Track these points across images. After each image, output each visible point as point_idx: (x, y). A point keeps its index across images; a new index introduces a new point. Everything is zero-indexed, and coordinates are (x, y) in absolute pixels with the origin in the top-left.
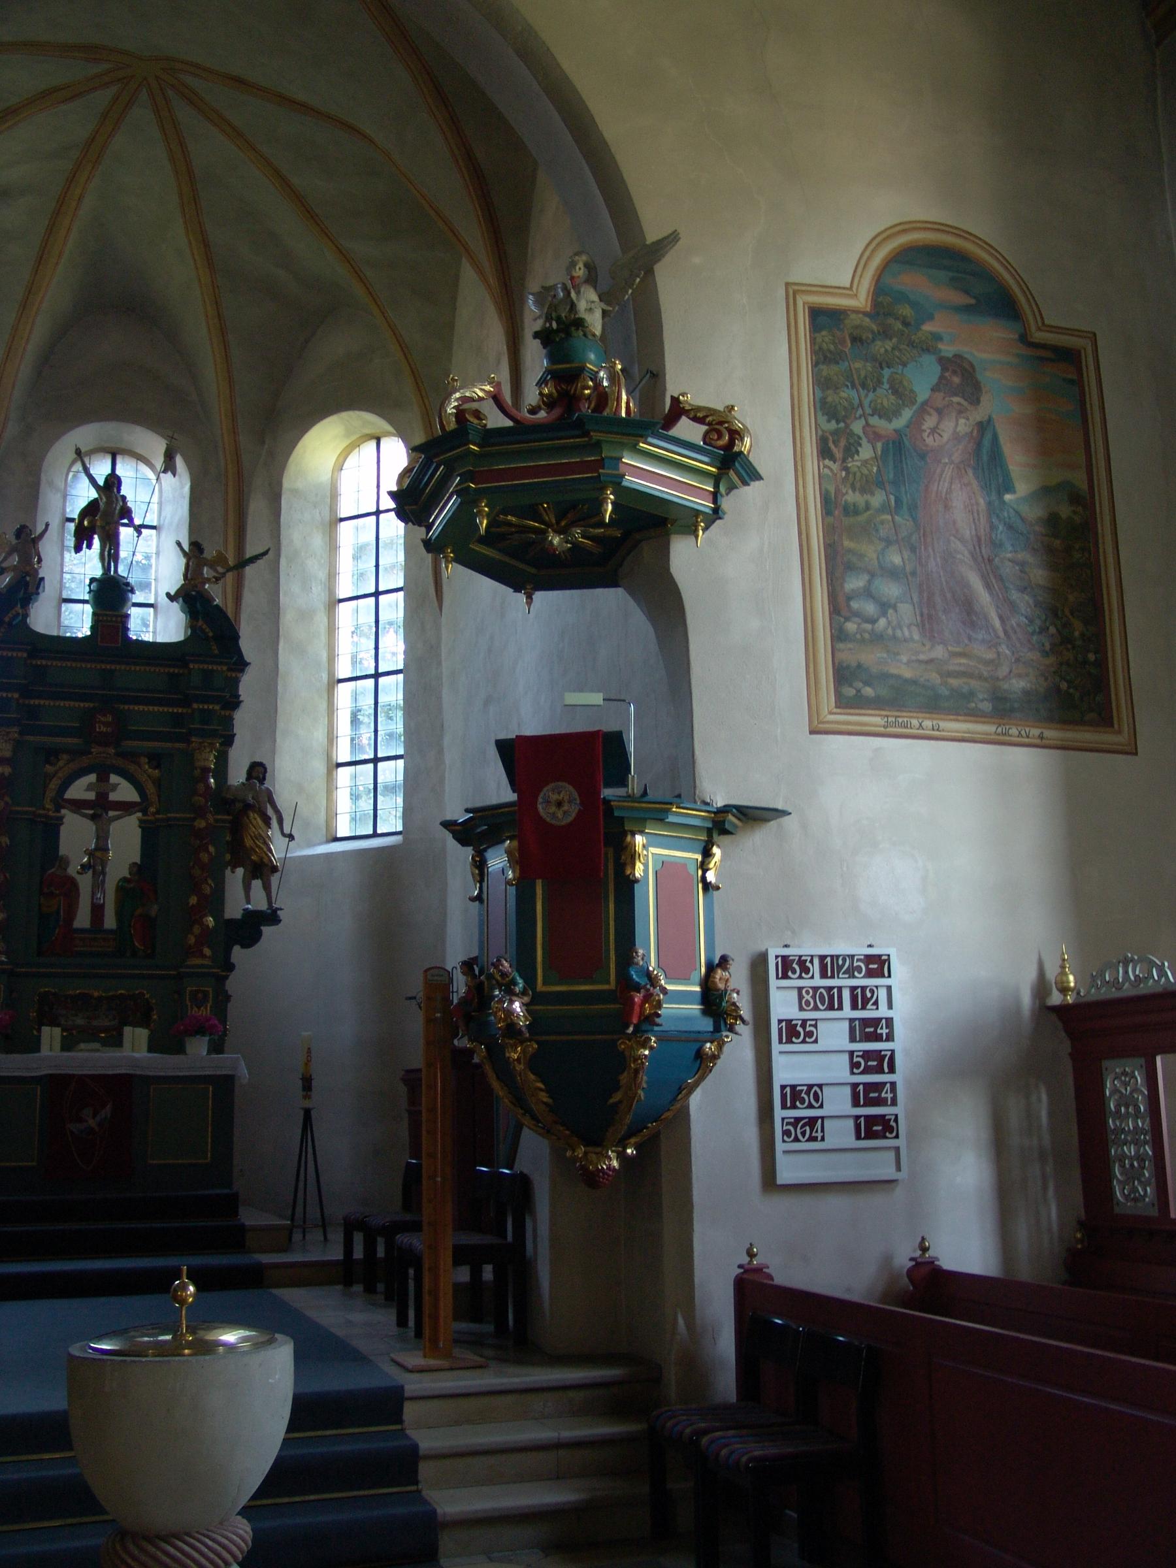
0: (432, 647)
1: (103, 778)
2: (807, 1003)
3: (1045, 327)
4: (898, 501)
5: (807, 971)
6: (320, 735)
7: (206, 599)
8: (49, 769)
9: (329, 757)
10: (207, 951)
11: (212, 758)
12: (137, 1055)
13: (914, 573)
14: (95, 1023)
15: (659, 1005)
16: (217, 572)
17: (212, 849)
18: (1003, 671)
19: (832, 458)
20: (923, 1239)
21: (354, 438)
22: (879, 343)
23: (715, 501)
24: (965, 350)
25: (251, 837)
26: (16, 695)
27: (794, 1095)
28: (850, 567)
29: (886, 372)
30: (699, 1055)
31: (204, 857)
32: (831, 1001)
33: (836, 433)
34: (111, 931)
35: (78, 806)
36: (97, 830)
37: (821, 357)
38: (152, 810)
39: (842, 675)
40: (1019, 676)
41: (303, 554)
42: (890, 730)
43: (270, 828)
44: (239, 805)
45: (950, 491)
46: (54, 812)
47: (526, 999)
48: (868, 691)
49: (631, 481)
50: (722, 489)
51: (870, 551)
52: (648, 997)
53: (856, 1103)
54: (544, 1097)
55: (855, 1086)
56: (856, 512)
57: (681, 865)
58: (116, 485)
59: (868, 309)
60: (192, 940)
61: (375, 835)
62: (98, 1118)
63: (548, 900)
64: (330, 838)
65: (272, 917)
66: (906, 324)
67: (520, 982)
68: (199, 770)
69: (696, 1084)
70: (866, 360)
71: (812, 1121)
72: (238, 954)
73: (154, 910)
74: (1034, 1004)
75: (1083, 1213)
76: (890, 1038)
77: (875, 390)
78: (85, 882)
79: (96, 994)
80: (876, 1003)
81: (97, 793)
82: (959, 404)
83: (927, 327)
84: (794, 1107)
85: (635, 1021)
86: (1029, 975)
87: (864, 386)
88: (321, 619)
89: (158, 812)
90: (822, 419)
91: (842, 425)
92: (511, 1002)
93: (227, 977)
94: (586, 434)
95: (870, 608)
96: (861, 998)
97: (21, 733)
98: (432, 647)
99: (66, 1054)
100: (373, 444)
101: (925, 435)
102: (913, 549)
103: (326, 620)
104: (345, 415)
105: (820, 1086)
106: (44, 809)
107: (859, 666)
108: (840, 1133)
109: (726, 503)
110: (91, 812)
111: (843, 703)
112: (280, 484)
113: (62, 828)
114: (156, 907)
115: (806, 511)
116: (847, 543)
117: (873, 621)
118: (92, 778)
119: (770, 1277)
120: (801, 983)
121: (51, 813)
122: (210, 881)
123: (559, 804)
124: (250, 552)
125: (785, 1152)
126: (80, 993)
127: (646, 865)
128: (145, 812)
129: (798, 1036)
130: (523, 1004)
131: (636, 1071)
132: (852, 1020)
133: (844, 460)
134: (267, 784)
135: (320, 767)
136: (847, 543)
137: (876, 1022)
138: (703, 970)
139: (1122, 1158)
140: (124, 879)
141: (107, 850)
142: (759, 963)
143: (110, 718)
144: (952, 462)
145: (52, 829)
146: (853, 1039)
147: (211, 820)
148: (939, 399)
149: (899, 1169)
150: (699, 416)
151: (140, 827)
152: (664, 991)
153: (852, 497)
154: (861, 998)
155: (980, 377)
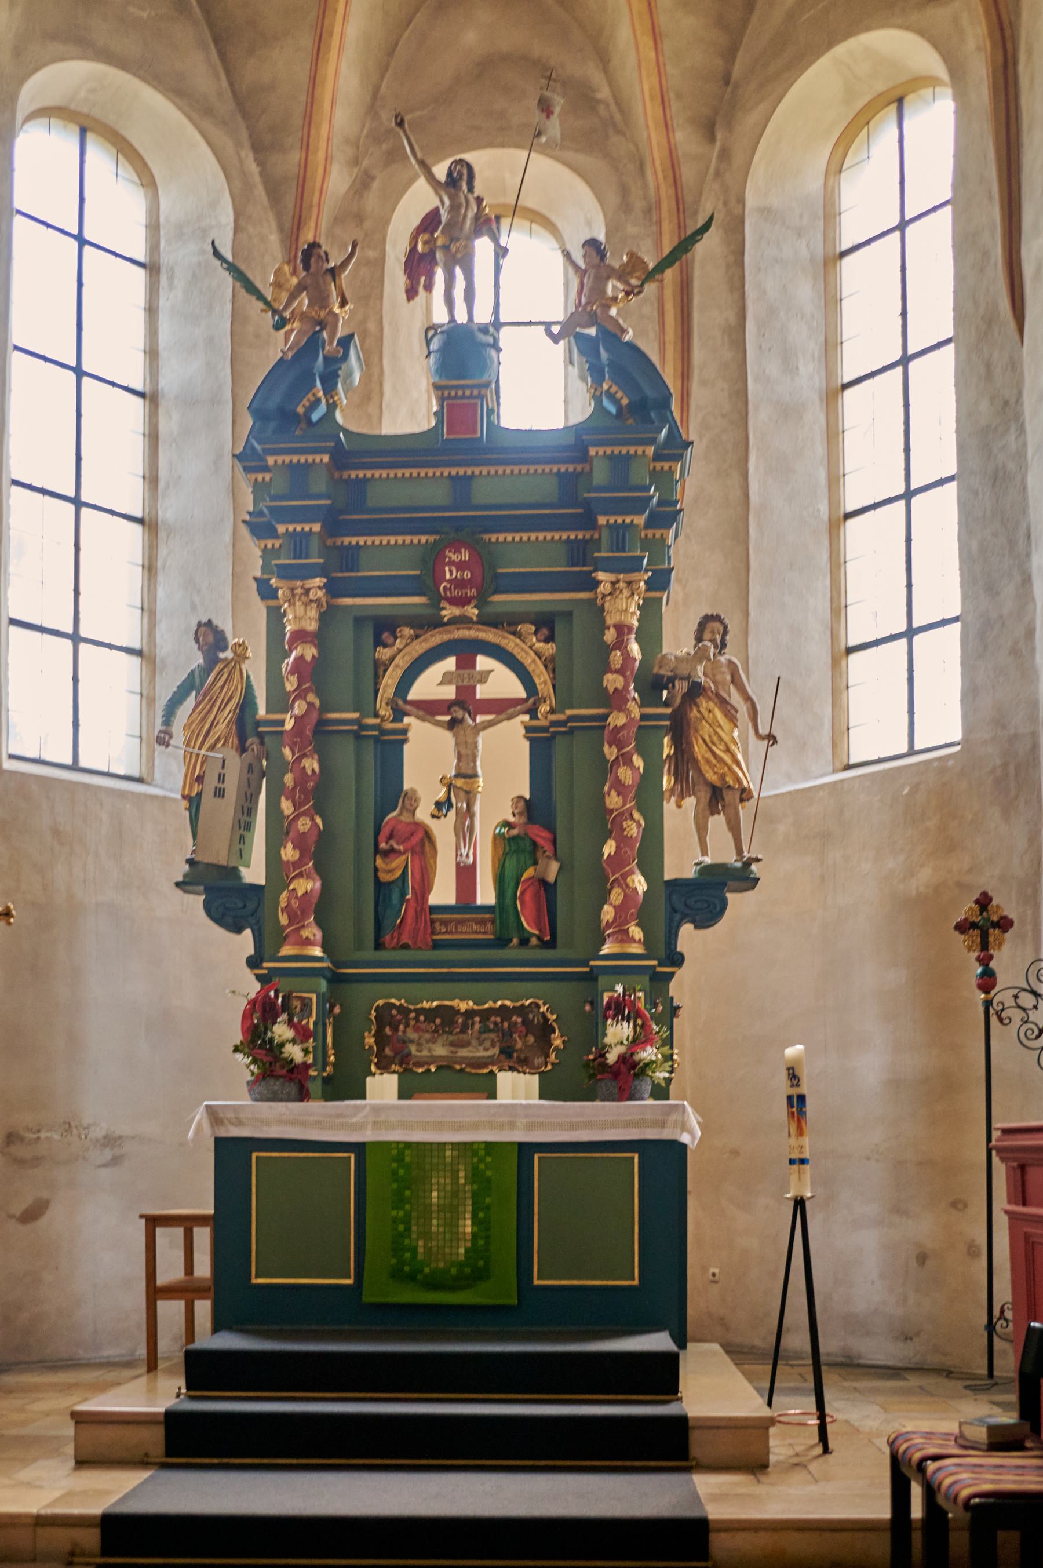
0: (1006, 403)
1: (466, 663)
7: (611, 335)
8: (383, 653)
11: (633, 608)
14: (463, 1053)
16: (627, 283)
25: (705, 742)
26: (317, 527)
31: (625, 774)
38: (544, 708)
41: (782, 314)
43: (736, 726)
44: (681, 687)
46: (393, 721)
58: (465, 177)
61: (912, 752)
64: (838, 765)
68: (612, 630)
72: (688, 936)
73: (552, 870)
78: (443, 830)
79: (463, 1006)
81: (458, 688)
88: (815, 415)
89: (552, 711)
93: (671, 975)
97: (333, 589)
98: (1006, 403)
103: (822, 418)
106: (376, 715)
110: (447, 718)
113: (406, 747)
114: (554, 866)
118: (450, 663)
122: (637, 815)
126: (437, 1007)
128: (533, 712)
135: (819, 652)
141: (475, 776)
143: (465, 556)
151: (527, 738)
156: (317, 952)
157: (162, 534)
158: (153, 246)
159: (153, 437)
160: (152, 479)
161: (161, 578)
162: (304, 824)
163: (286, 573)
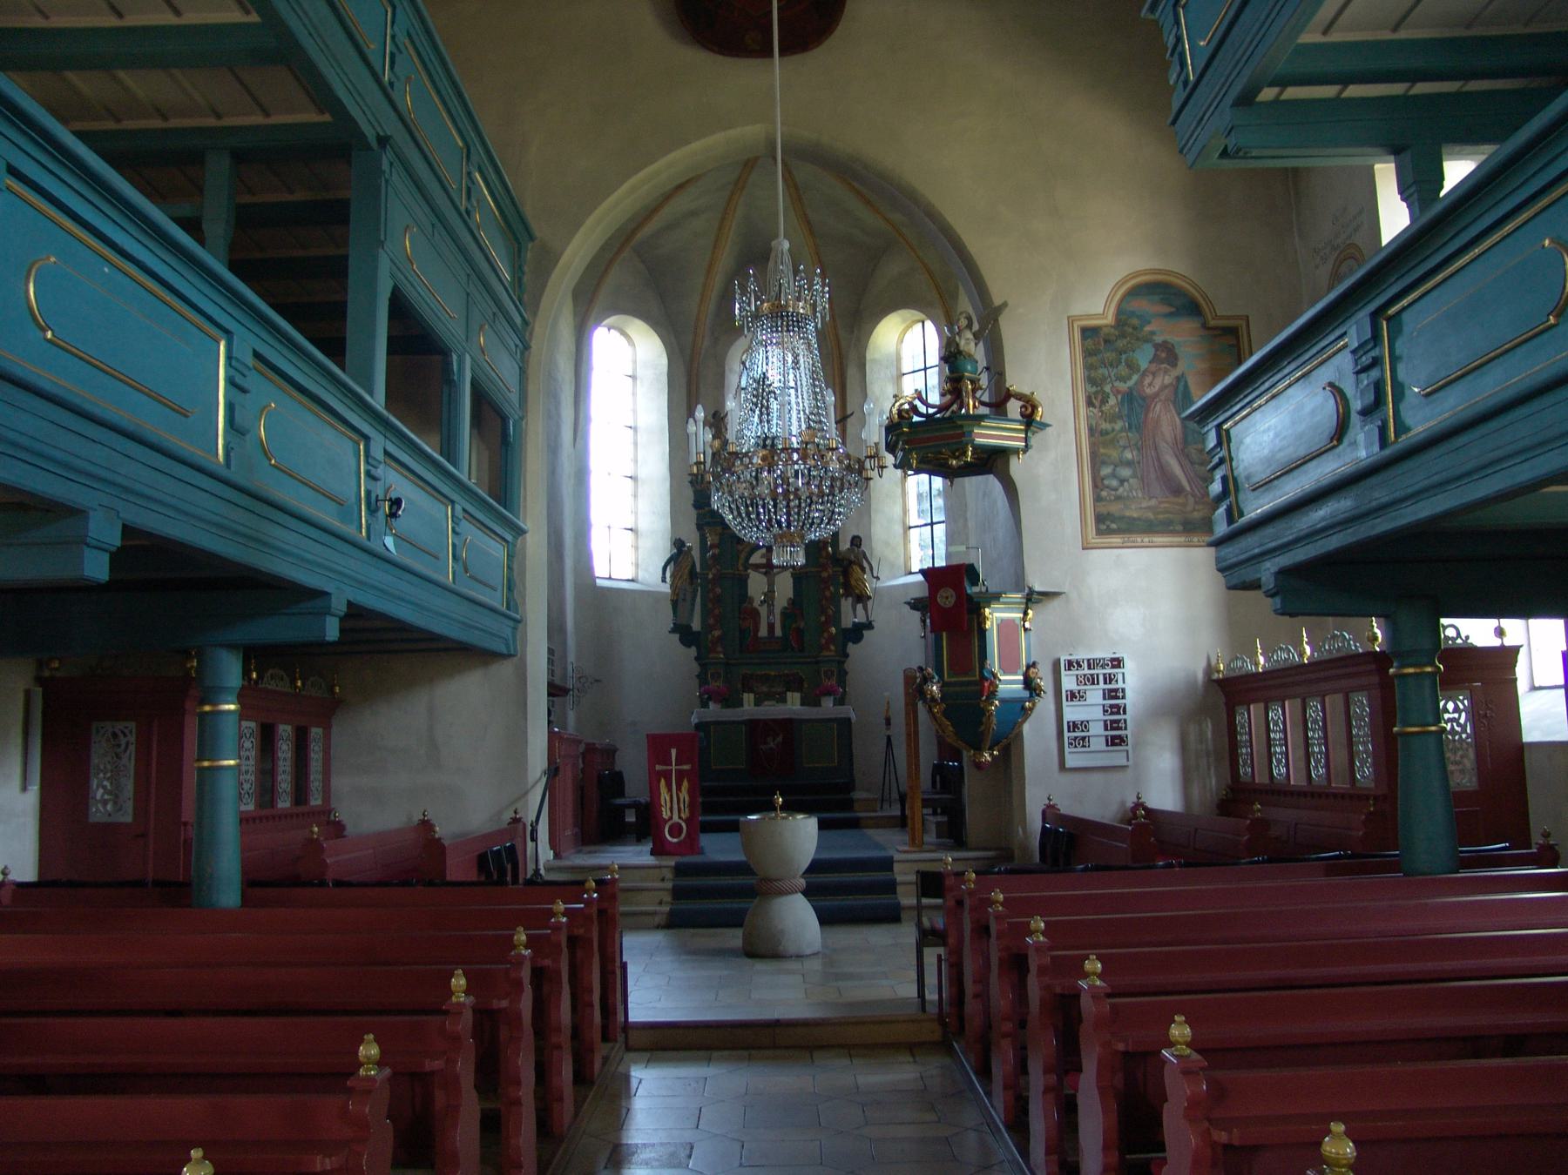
2: (1081, 682)
3: (1216, 317)
4: (1130, 427)
5: (1081, 667)
6: (898, 510)
9: (904, 523)
10: (833, 648)
12: (794, 708)
13: (1139, 463)
14: (773, 690)
15: (997, 686)
17: (832, 588)
18: (1189, 508)
19: (1094, 406)
20: (1138, 794)
21: (908, 323)
22: (1119, 341)
23: (1026, 442)
24: (1168, 338)
27: (1074, 726)
28: (1104, 463)
29: (1124, 356)
30: (1023, 708)
31: (827, 593)
32: (1093, 680)
33: (1096, 393)
34: (778, 638)
35: (757, 567)
36: (768, 580)
37: (1088, 353)
39: (1100, 519)
40: (1198, 510)
42: (1125, 545)
45: (1159, 416)
47: (939, 685)
48: (1114, 526)
49: (979, 440)
50: (1029, 434)
51: (1114, 454)
52: (992, 683)
53: (1106, 729)
54: (951, 729)
55: (1105, 721)
56: (1107, 433)
57: (1012, 621)
59: (1113, 324)
60: (823, 641)
62: (776, 742)
63: (948, 638)
65: (869, 625)
66: (1135, 328)
67: (937, 678)
69: (1024, 721)
70: (1112, 351)
71: (1083, 738)
72: (851, 648)
73: (802, 625)
74: (1204, 678)
75: (1230, 781)
76: (1124, 697)
77: (1117, 367)
78: (763, 611)
79: (773, 673)
80: (1117, 681)
82: (1165, 368)
83: (1147, 328)
84: (1074, 731)
85: (986, 694)
86: (1202, 665)
87: (1111, 365)
90: (1089, 387)
91: (1099, 388)
92: (932, 687)
94: (954, 422)
95: (1114, 483)
96: (1109, 679)
99: (756, 708)
100: (920, 324)
101: (1145, 388)
102: (1138, 449)
104: (900, 312)
105: (1088, 722)
107: (1108, 514)
108: (1098, 744)
109: (1034, 441)
111: (1099, 533)
112: (865, 357)
113: (749, 581)
115: (1080, 436)
116: (1102, 450)
117: (1116, 490)
119: (1059, 810)
120: (1077, 672)
121: (743, 573)
123: (947, 598)
124: (849, 412)
125: (1070, 753)
127: (992, 623)
129: (1076, 698)
130: (937, 687)
131: (989, 716)
132: (1104, 690)
133: (1100, 407)
134: (863, 548)
135: (898, 529)
136: (1102, 450)
137: (1116, 690)
138: (1024, 668)
139: (1242, 754)
140: (785, 608)
142: (1057, 664)
144: (1160, 400)
145: (743, 581)
146: (1104, 698)
147: (830, 571)
148: (1154, 367)
149: (1128, 760)
150: (1019, 397)
152: (1000, 680)
153: (1105, 426)
154: (1109, 679)
155: (1177, 351)
156: (722, 656)
157: (639, 483)
158: (635, 369)
159: (636, 444)
160: (636, 461)
161: (640, 500)
162: (717, 612)
163: (708, 524)
